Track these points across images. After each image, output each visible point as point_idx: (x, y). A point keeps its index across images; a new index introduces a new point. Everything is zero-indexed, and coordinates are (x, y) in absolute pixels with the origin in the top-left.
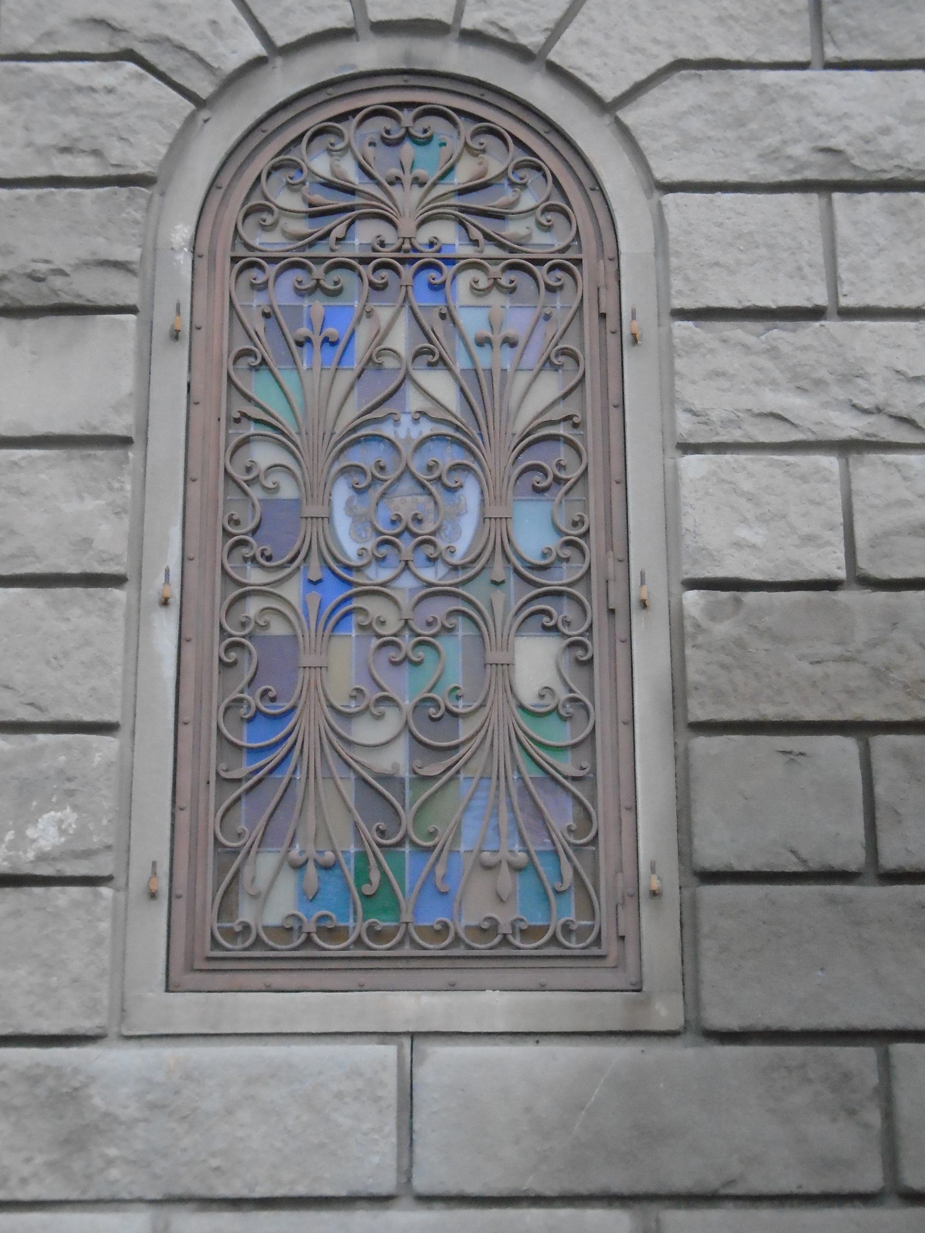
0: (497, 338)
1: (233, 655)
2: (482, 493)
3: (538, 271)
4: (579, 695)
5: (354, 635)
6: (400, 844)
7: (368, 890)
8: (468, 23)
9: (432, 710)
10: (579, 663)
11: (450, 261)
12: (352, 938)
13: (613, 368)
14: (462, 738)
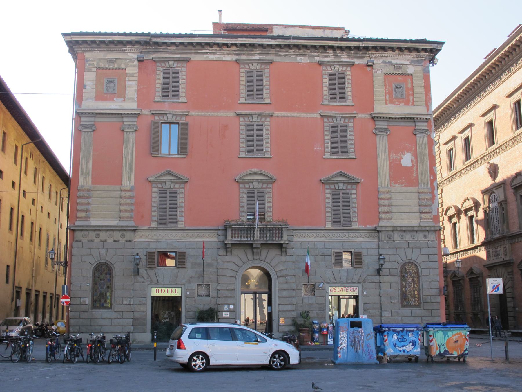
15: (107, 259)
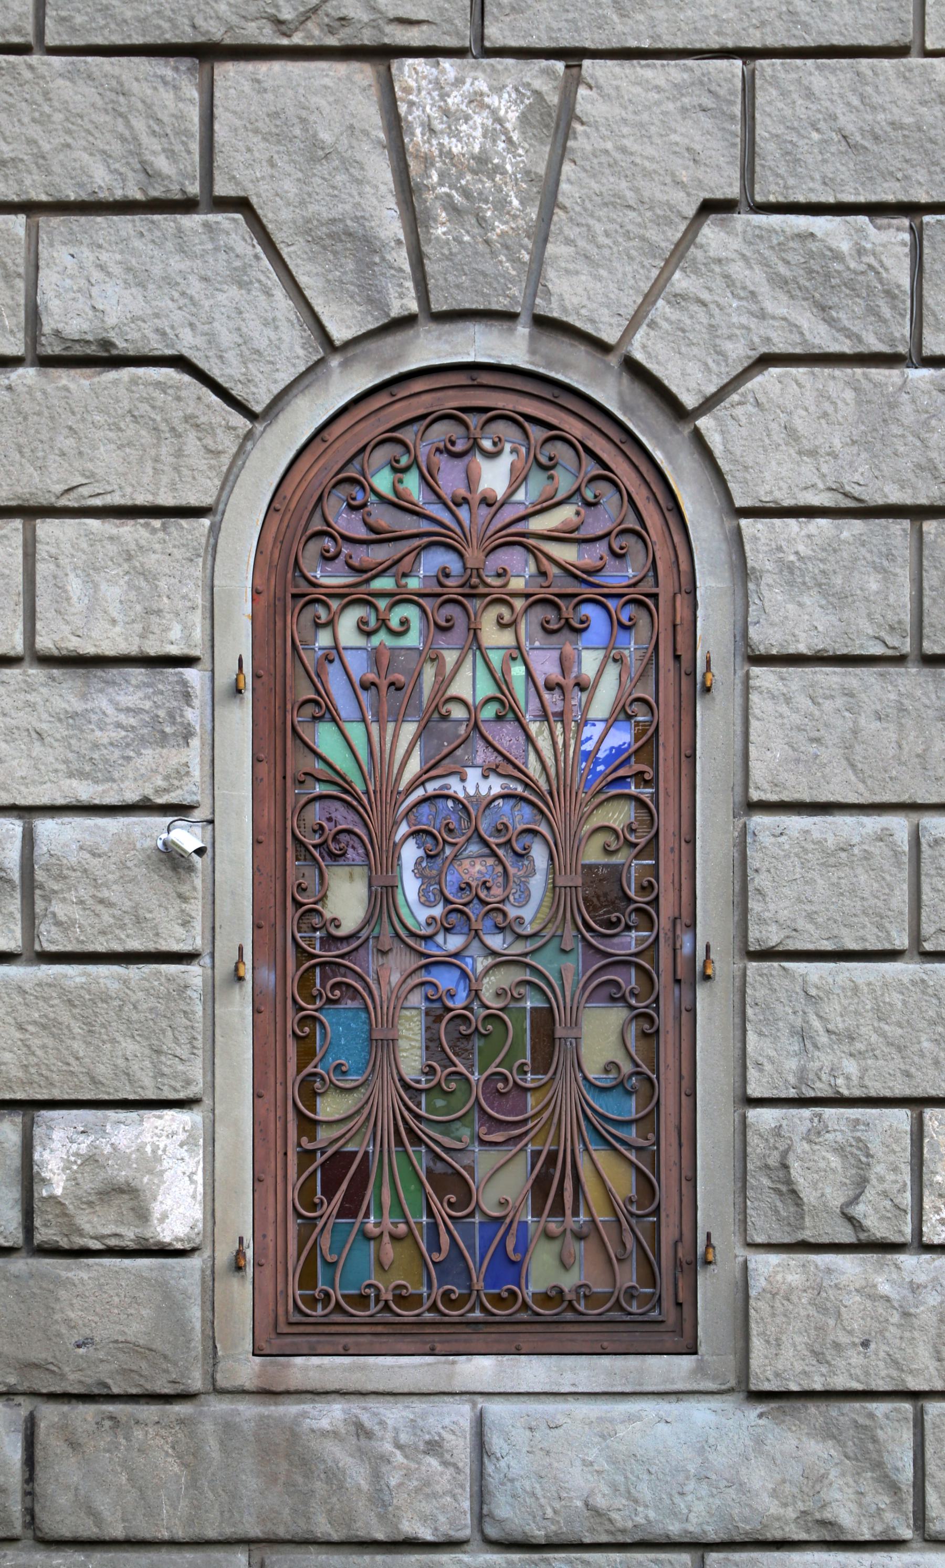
0: (569, 682)
2: (551, 858)
3: (611, 604)
4: (645, 1069)
6: (471, 1215)
7: (438, 1258)
9: (500, 1085)
10: (645, 1035)
12: (427, 1304)
13: (686, 719)
14: (530, 1113)
15: (573, 293)
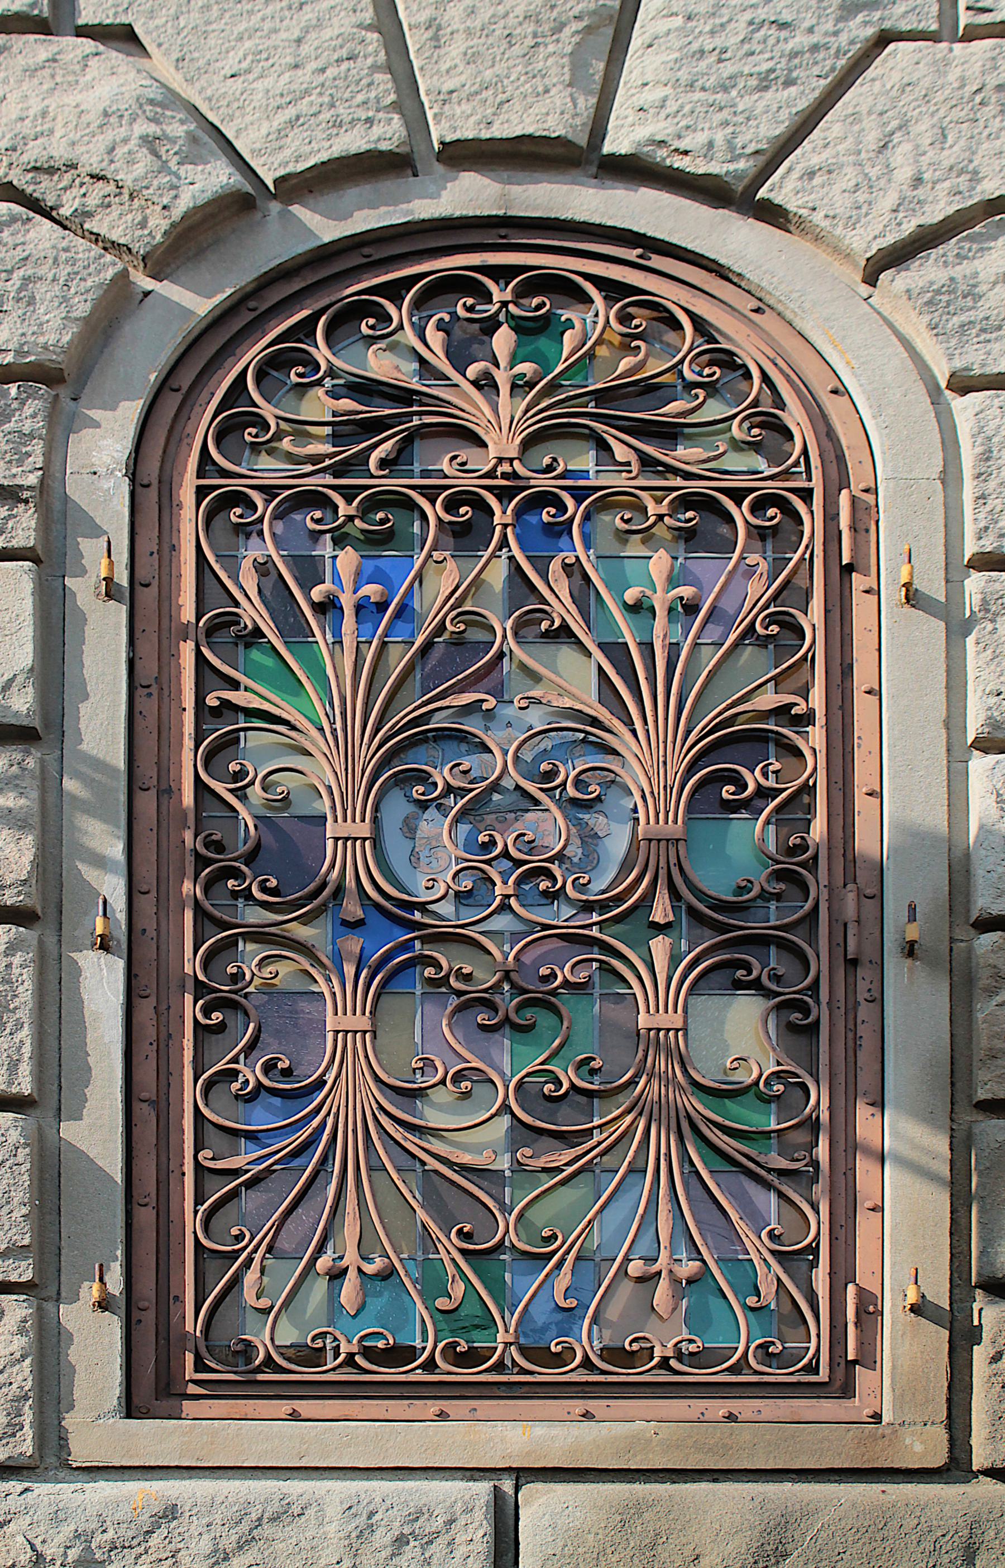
1: (217, 1017)
5: (418, 993)
8: (618, 142)
11: (579, 494)
